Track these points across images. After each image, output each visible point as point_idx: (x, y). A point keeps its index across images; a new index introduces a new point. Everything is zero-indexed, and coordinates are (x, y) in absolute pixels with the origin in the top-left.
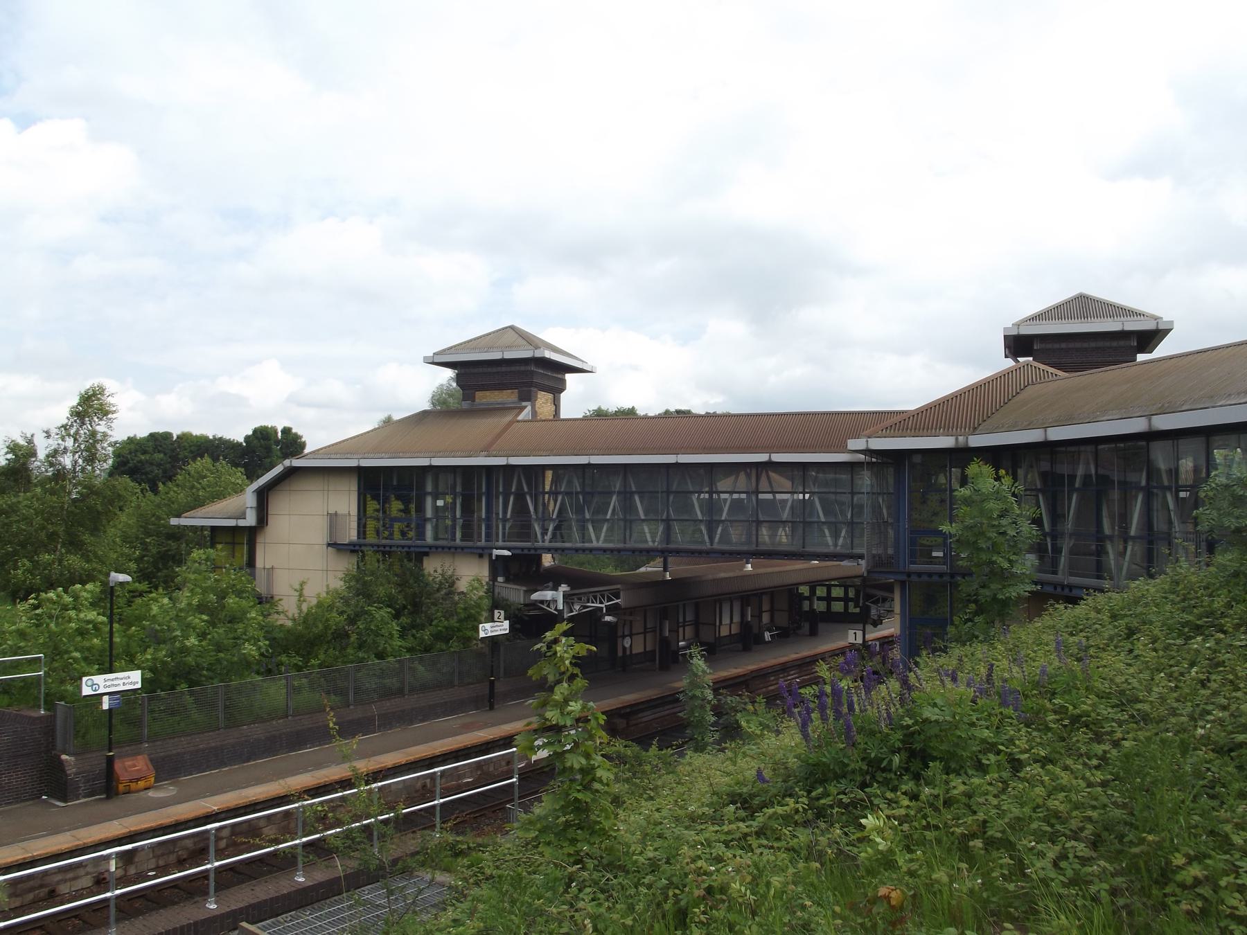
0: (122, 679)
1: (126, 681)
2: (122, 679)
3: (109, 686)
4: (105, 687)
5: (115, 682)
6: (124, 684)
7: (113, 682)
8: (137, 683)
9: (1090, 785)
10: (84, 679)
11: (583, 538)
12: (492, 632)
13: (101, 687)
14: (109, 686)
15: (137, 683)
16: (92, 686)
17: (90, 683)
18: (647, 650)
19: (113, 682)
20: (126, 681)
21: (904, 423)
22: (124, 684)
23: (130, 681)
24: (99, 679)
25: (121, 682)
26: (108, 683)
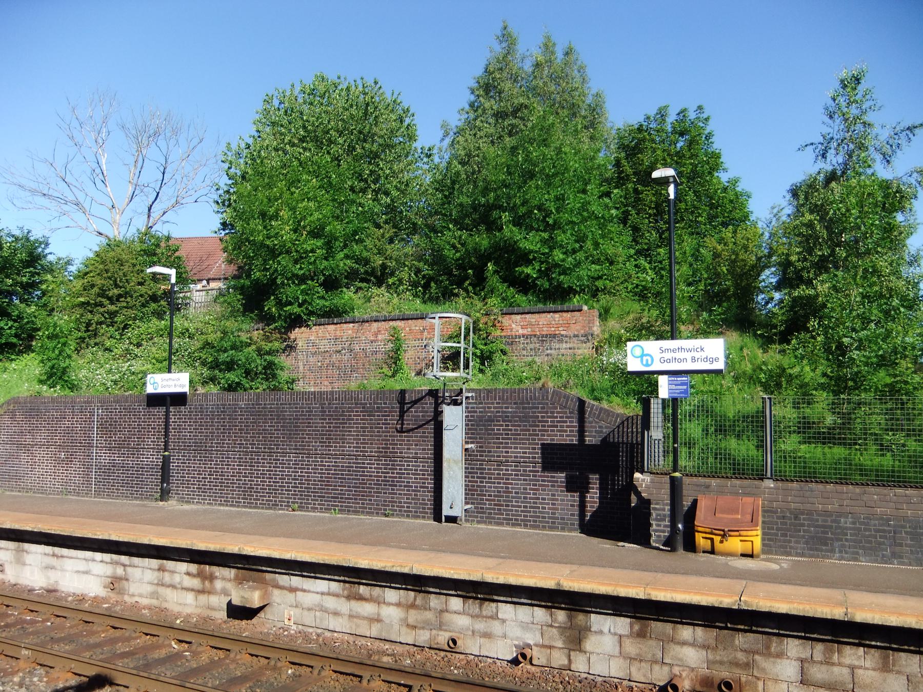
0: (690, 350)
1: (697, 355)
2: (690, 350)
3: (669, 361)
4: (662, 360)
5: (678, 355)
6: (694, 359)
7: (674, 355)
8: (717, 359)
9: (840, 473)
10: (149, 376)
11: (632, 452)
12: (163, 387)
13: (656, 360)
14: (669, 361)
15: (717, 359)
16: (642, 356)
17: (638, 352)
18: (588, 440)
19: (674, 355)
20: (697, 355)
21: (618, 432)
22: (694, 359)
23: (704, 355)
24: (652, 347)
25: (688, 355)
26: (165, 383)
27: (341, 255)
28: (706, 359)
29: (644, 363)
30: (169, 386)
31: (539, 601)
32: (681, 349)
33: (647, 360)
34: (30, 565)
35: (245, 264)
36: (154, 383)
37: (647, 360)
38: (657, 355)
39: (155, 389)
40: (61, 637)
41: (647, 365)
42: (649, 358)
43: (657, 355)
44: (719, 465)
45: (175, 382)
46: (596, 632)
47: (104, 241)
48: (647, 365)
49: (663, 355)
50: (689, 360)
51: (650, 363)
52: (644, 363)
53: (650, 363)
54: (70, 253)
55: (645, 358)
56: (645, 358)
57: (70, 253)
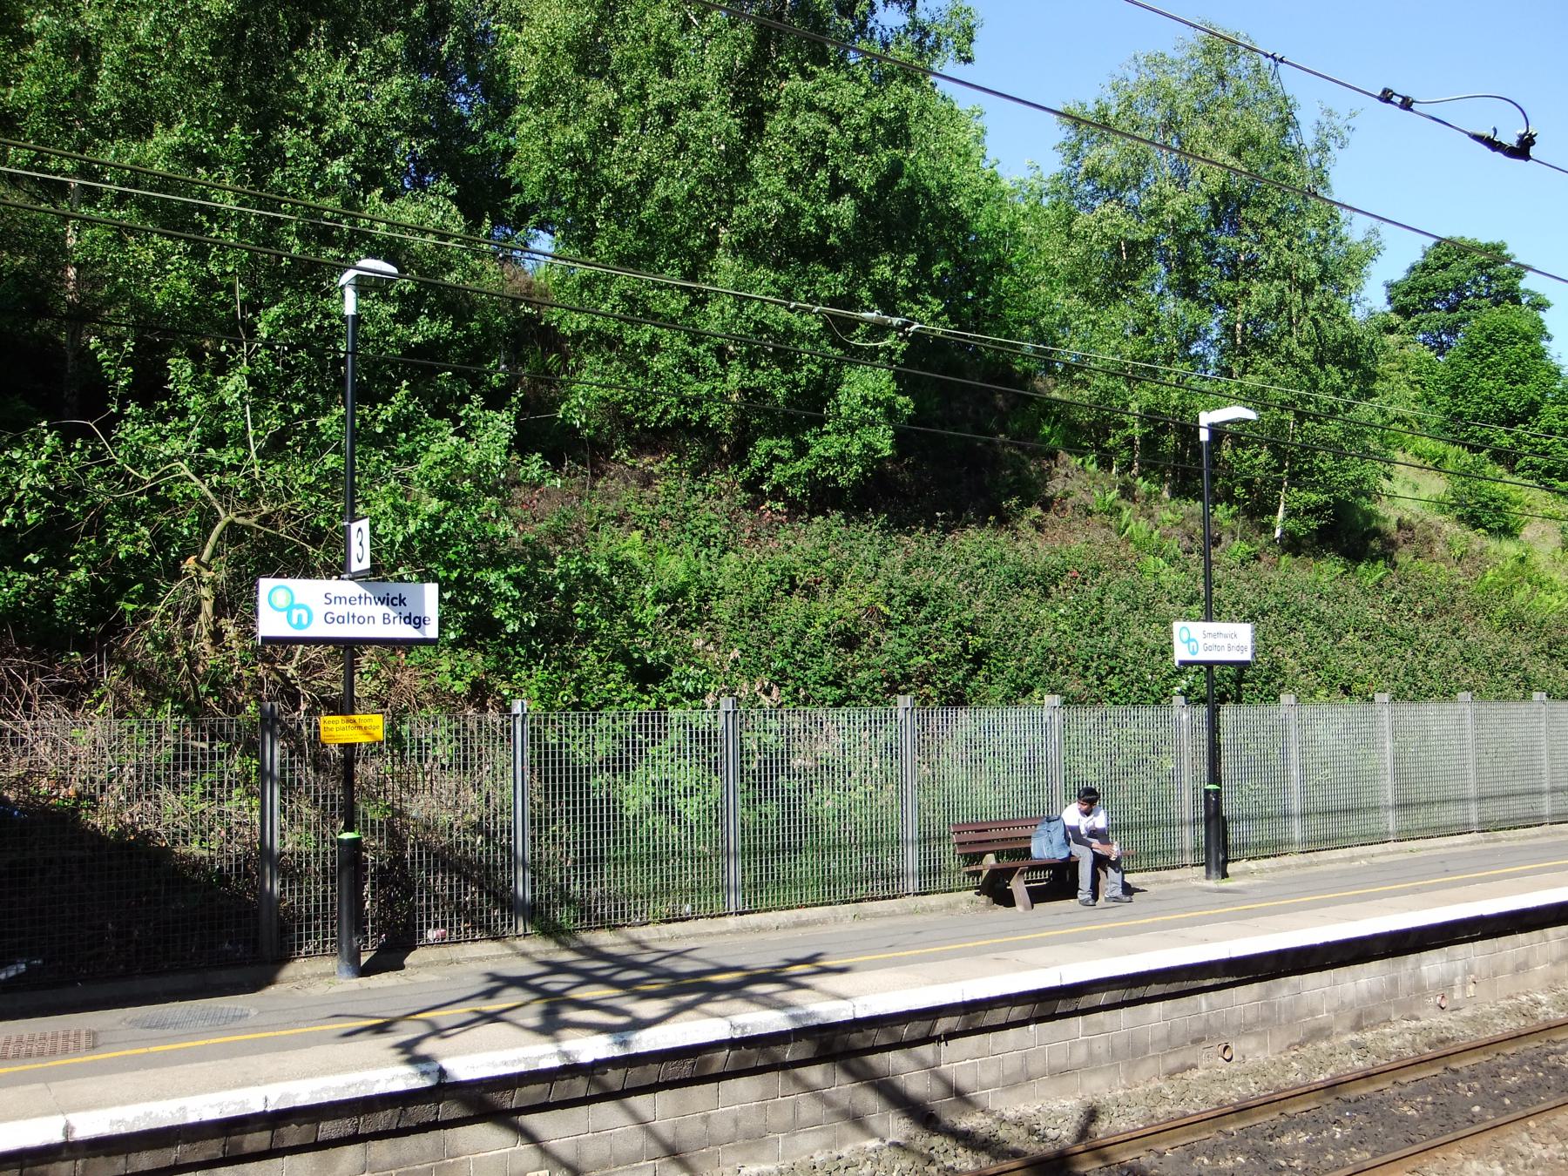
3: (341, 620)
5: (1220, 641)
12: (1208, 648)
14: (341, 620)
17: (281, 599)
26: (1210, 641)
30: (1219, 648)
33: (300, 617)
34: (211, 1107)
35: (372, 140)
37: (300, 617)
38: (320, 609)
44: (542, 728)
45: (1229, 641)
46: (1214, 728)
47: (1430, 242)
48: (299, 626)
49: (331, 608)
50: (379, 619)
51: (305, 621)
52: (295, 621)
53: (305, 621)
54: (1424, 247)
55: (295, 613)
57: (1424, 247)
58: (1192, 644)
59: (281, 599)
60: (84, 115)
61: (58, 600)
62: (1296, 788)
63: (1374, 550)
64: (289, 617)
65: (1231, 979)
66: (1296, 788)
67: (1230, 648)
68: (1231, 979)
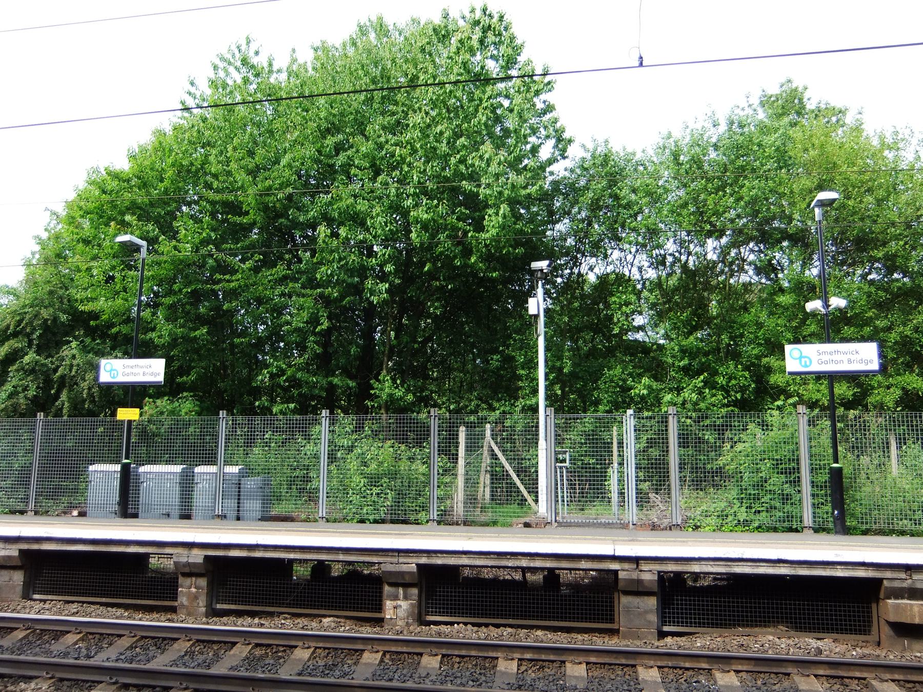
1: (147, 371)
3: (826, 362)
5: (135, 370)
6: (850, 361)
7: (831, 357)
8: (871, 361)
15: (871, 361)
17: (796, 354)
19: (831, 357)
22: (850, 361)
23: (859, 357)
26: (128, 370)
27: (165, 258)
28: (861, 361)
29: (803, 364)
31: (682, 624)
32: (137, 366)
33: (806, 362)
36: (112, 370)
37: (806, 362)
39: (113, 378)
40: (896, 598)
41: (806, 366)
42: (115, 372)
43: (121, 370)
45: (849, 356)
48: (806, 366)
49: (821, 357)
50: (846, 361)
51: (808, 364)
52: (803, 364)
53: (808, 364)
55: (803, 360)
56: (803, 360)
58: (113, 372)
59: (796, 354)
60: (576, 245)
61: (191, 326)
62: (39, 431)
63: (467, 356)
64: (801, 361)
65: (233, 607)
66: (39, 431)
67: (144, 374)
68: (233, 607)
